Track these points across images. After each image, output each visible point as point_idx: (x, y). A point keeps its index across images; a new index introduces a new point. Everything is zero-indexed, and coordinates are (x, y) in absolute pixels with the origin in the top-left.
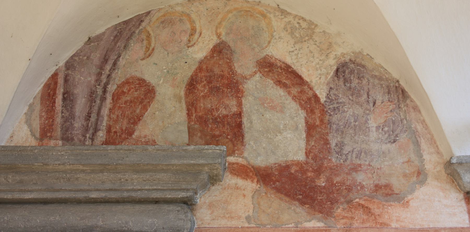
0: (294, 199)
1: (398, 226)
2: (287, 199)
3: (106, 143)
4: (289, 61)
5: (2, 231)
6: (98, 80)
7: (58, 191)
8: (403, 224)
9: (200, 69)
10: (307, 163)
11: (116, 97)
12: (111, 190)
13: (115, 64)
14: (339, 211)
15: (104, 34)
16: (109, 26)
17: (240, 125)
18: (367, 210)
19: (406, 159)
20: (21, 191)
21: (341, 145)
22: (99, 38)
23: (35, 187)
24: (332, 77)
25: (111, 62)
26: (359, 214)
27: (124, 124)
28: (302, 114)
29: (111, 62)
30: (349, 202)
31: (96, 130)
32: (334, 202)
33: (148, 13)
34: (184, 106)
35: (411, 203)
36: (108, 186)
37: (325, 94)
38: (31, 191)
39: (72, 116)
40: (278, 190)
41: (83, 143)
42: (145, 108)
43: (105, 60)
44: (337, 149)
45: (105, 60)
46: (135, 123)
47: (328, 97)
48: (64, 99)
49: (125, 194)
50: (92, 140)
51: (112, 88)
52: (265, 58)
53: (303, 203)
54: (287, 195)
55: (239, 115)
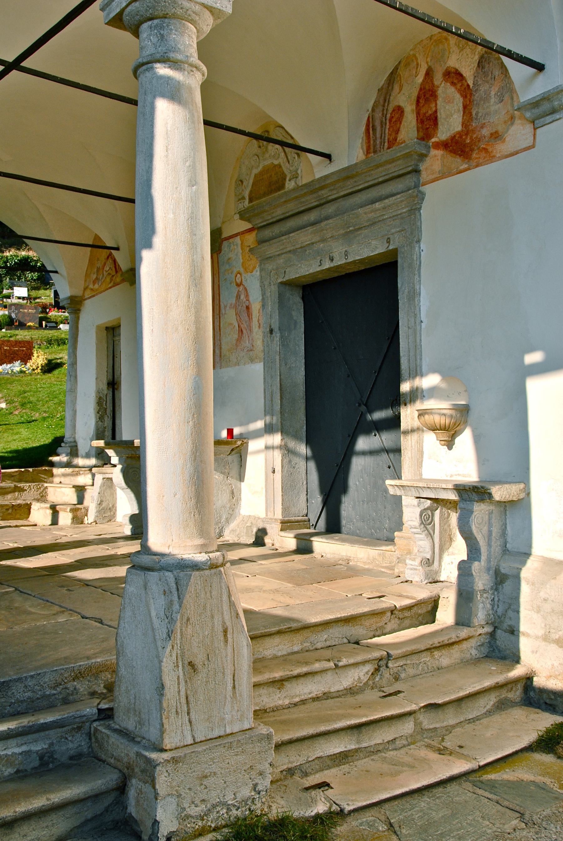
0: (457, 154)
1: (499, 155)
2: (454, 155)
3: (389, 148)
4: (457, 66)
5: (3, 405)
6: (383, 114)
7: (369, 181)
8: (501, 153)
9: (421, 89)
10: (462, 131)
11: (390, 121)
12: (385, 175)
13: (389, 101)
14: (474, 155)
15: (383, 85)
16: (385, 78)
17: (436, 118)
18: (485, 150)
19: (506, 111)
20: (357, 186)
21: (477, 114)
22: (382, 88)
23: (361, 183)
24: (476, 69)
25: (387, 101)
26: (483, 154)
27: (393, 135)
28: (461, 99)
29: (387, 101)
30: (478, 149)
31: (384, 143)
32: (472, 150)
33: (400, 62)
34: (415, 115)
35: (506, 139)
36: (384, 173)
37: (472, 82)
38: (361, 184)
39: (376, 138)
40: (451, 151)
41: (380, 151)
42: (401, 123)
43: (385, 100)
44: (476, 117)
45: (385, 100)
46: (397, 133)
47: (473, 84)
48: (373, 130)
49: (391, 176)
50: (383, 148)
51: (388, 116)
52: (446, 69)
53: (460, 156)
54: (454, 153)
55: (436, 112)
